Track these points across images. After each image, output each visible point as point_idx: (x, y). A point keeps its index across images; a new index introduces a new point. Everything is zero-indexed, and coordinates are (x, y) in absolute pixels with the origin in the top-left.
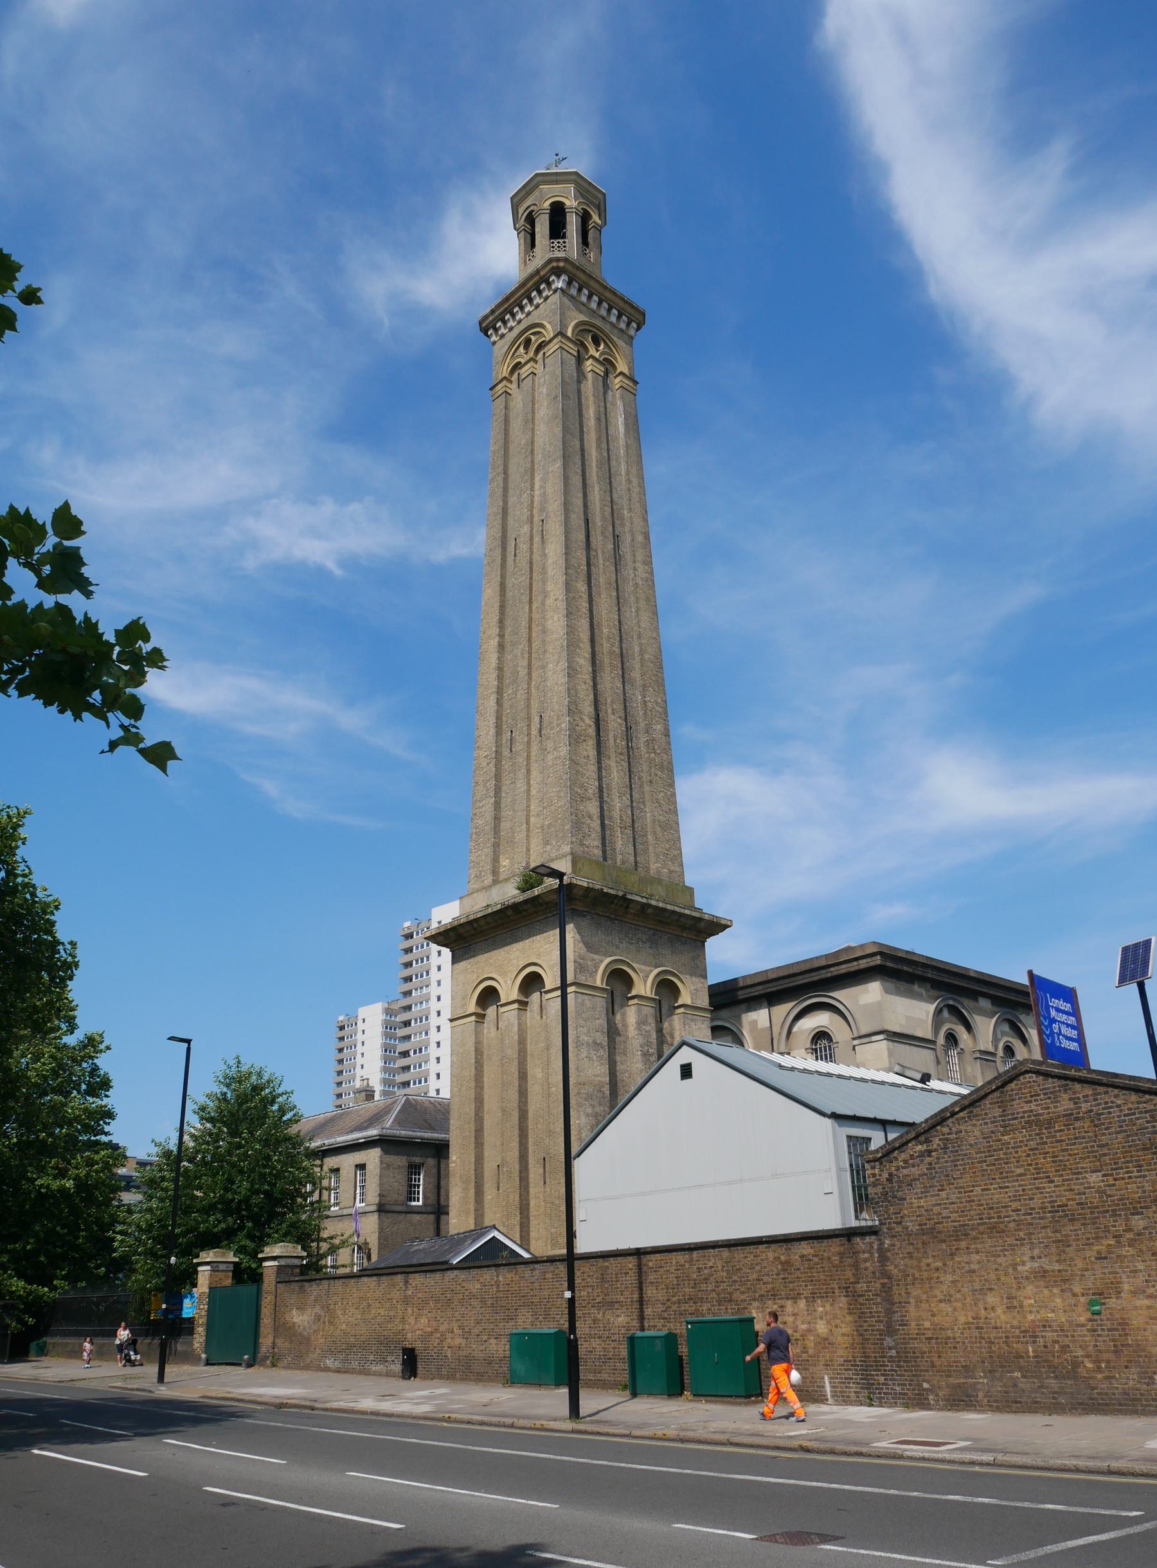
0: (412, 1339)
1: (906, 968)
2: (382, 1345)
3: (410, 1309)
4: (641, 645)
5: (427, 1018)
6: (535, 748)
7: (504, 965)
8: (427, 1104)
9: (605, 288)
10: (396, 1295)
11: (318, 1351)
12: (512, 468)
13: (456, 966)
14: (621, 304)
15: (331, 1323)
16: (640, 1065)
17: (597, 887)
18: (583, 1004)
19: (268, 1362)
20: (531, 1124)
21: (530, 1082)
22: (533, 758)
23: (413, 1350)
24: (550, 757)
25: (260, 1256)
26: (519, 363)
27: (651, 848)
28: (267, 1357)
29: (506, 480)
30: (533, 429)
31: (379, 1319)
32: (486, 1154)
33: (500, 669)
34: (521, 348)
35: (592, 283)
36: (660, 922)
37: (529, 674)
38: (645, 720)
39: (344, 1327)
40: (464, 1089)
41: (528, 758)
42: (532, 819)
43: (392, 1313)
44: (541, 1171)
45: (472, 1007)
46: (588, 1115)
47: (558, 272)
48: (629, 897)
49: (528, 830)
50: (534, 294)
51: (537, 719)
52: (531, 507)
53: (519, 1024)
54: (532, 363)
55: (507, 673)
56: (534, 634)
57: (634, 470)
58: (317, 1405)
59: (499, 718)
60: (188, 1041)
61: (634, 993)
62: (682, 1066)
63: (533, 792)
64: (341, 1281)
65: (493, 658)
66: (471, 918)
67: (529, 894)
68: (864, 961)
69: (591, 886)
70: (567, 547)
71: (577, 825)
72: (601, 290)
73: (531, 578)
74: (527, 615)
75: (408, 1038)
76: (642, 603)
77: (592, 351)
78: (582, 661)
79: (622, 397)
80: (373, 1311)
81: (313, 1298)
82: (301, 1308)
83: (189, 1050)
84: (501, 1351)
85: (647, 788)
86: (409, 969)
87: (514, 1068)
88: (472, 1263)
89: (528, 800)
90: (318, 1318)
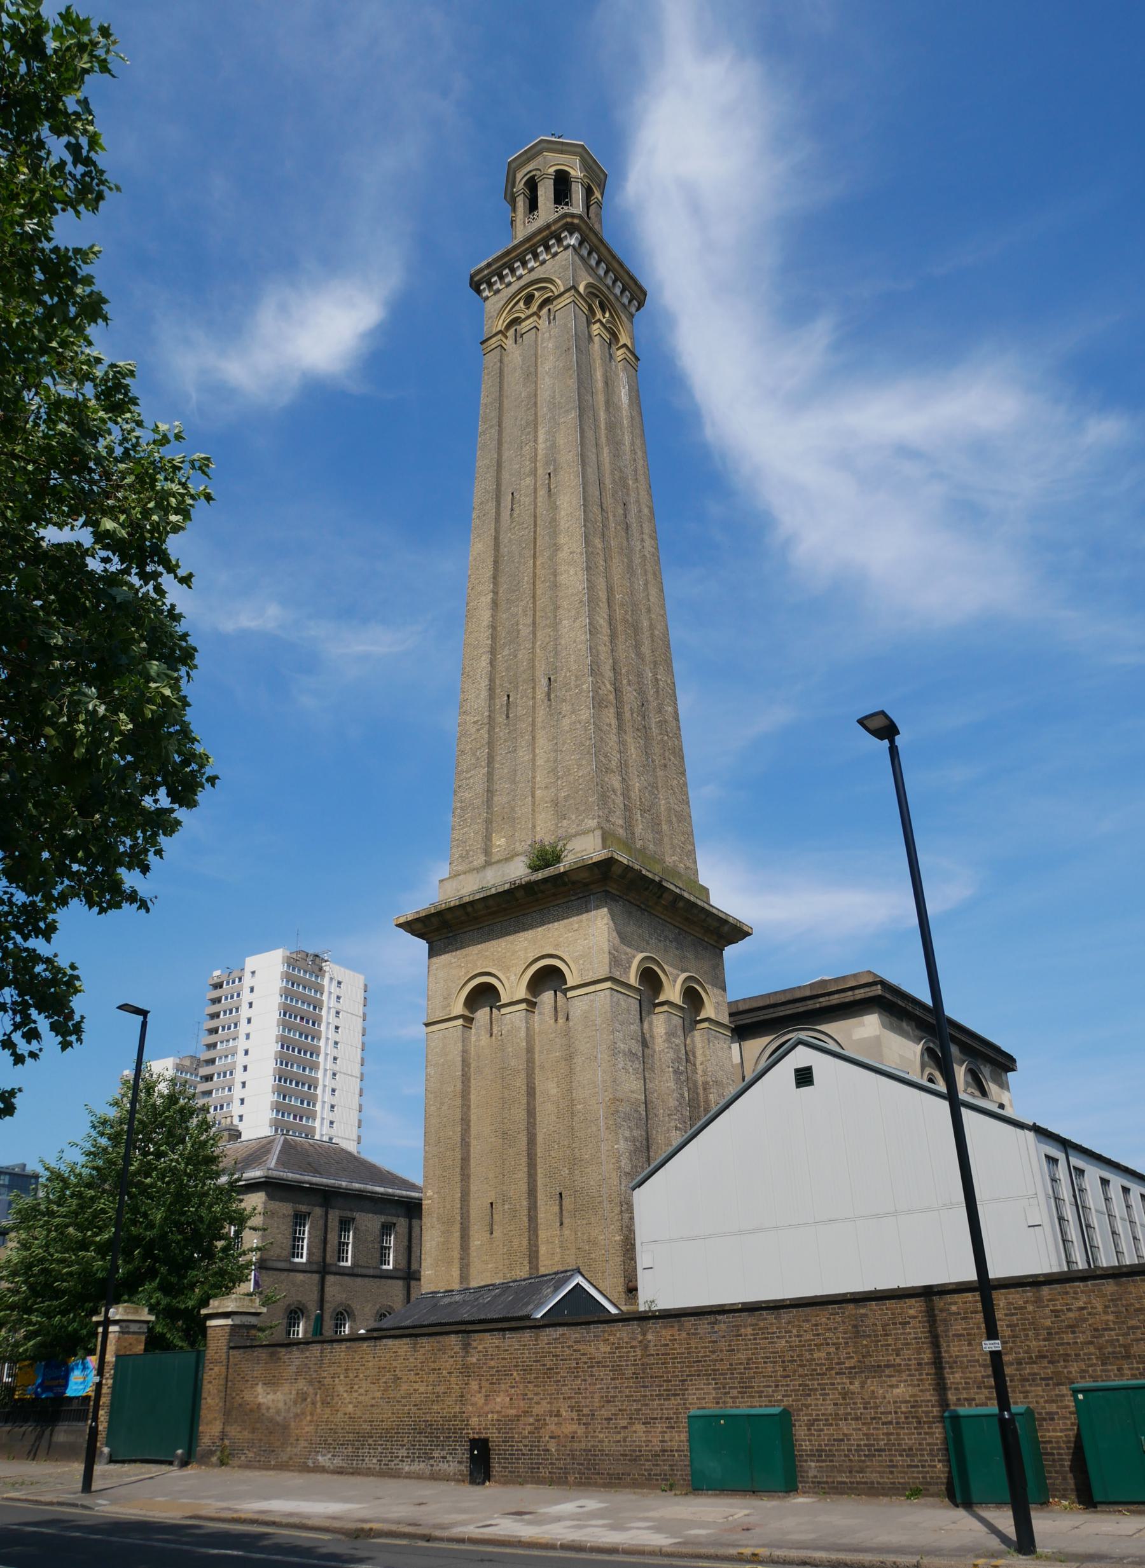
0: (477, 1426)
1: (900, 1003)
2: (711, 1432)
3: (474, 1385)
4: (650, 619)
5: (231, 1074)
6: (541, 713)
7: (509, 959)
9: (614, 257)
10: (446, 1363)
11: (303, 1443)
12: (508, 422)
13: (434, 960)
14: (626, 278)
15: (325, 1403)
16: (672, 1085)
17: (637, 867)
18: (618, 1003)
19: (214, 1459)
20: (540, 1151)
22: (539, 725)
23: (485, 1441)
24: (566, 722)
25: (204, 1312)
26: (519, 318)
27: (666, 840)
28: (212, 1453)
29: (500, 432)
30: (536, 383)
31: (415, 1398)
33: (493, 627)
34: (521, 304)
35: (602, 249)
36: (687, 919)
37: (534, 633)
38: (657, 699)
39: (350, 1409)
40: (445, 1107)
41: (533, 724)
42: (538, 793)
43: (440, 1389)
44: (557, 1209)
45: (458, 1008)
47: (571, 229)
48: (665, 884)
49: (534, 804)
50: (541, 249)
51: (544, 682)
52: (534, 459)
53: (528, 1028)
54: (535, 318)
55: (502, 632)
56: (539, 592)
57: (638, 442)
58: (438, 1533)
59: (492, 680)
60: (144, 1013)
61: (662, 998)
62: (797, 1071)
63: (540, 762)
64: (344, 1346)
65: (486, 616)
66: (466, 900)
67: (540, 875)
68: (862, 991)
69: (631, 864)
70: (584, 499)
71: (603, 798)
72: (610, 258)
73: (535, 532)
74: (531, 570)
75: (209, 1093)
76: (650, 576)
77: (599, 315)
78: (601, 621)
79: (625, 369)
80: (404, 1387)
81: (293, 1369)
82: (272, 1383)
83: (144, 1024)
84: (656, 1441)
85: (660, 773)
86: (219, 990)
87: (520, 1082)
88: (554, 1320)
89: (534, 771)
90: (302, 1397)
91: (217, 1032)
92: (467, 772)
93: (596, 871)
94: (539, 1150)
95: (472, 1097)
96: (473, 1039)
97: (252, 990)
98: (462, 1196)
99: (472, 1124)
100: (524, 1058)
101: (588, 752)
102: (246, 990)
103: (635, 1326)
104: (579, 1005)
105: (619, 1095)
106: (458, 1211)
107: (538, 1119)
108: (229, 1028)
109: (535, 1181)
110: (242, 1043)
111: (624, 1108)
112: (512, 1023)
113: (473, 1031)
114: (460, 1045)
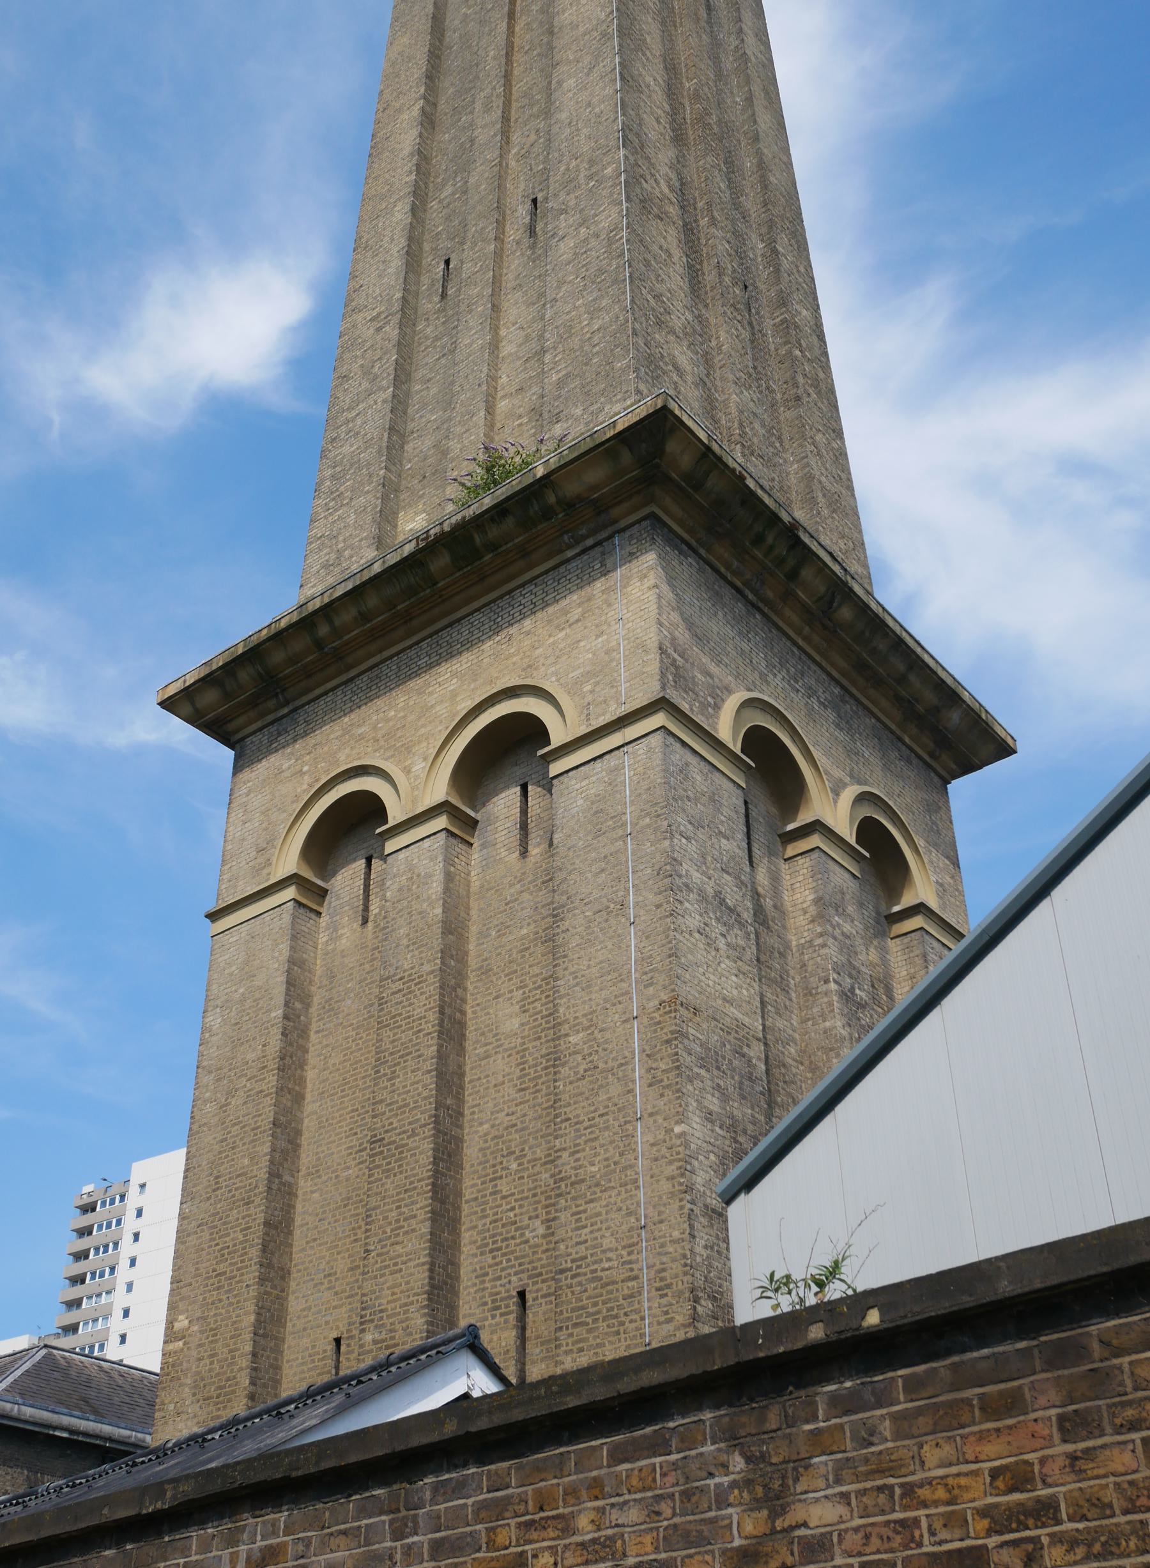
6: (514, 264)
8: (94, 1372)
13: (245, 775)
20: (470, 1185)
21: (473, 1049)
32: (295, 1304)
41: (496, 282)
42: (502, 406)
46: (709, 1117)
48: (802, 535)
51: (523, 211)
53: (449, 877)
63: (507, 349)
66: (311, 607)
74: (501, 39)
86: (90, 1215)
87: (424, 1007)
91: (83, 1282)
92: (350, 409)
93: (626, 457)
94: (467, 1182)
95: (311, 1074)
96: (323, 938)
97: (139, 1213)
98: (258, 1323)
99: (304, 1141)
100: (437, 943)
101: (616, 281)
102: (131, 1214)
103: (706, 1450)
104: (576, 791)
105: (688, 993)
106: (245, 1362)
107: (469, 1100)
108: (102, 1275)
109: (454, 1264)
110: (120, 1299)
111: (699, 1032)
112: (411, 869)
113: (324, 921)
114: (284, 948)
